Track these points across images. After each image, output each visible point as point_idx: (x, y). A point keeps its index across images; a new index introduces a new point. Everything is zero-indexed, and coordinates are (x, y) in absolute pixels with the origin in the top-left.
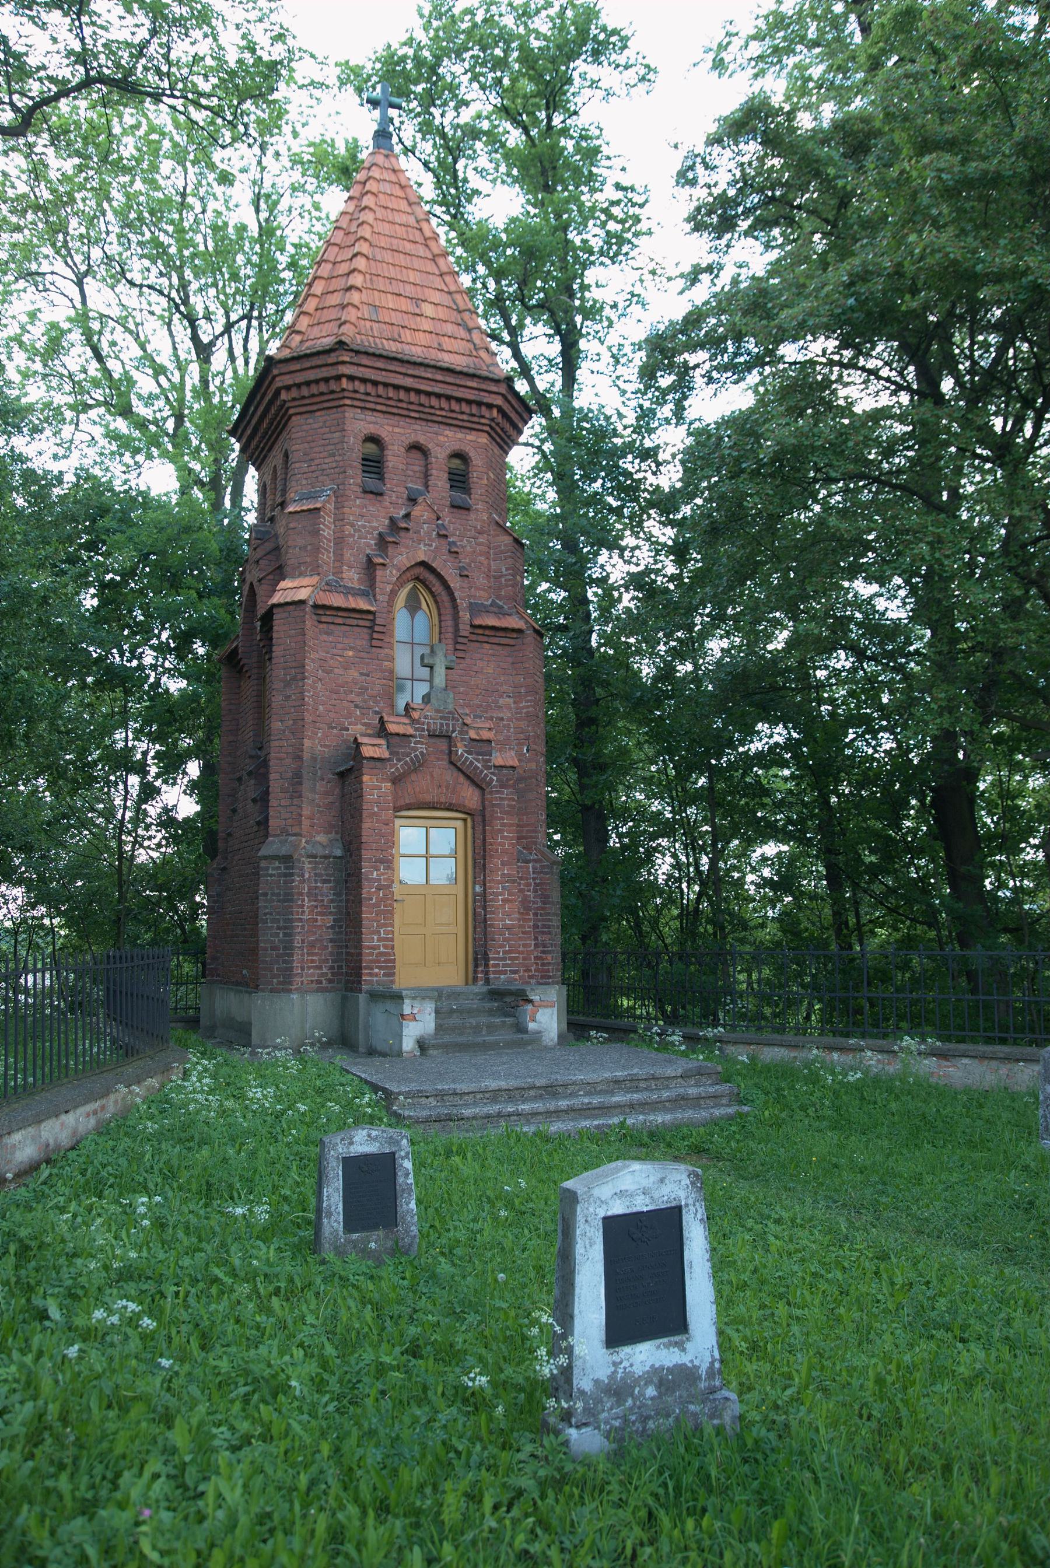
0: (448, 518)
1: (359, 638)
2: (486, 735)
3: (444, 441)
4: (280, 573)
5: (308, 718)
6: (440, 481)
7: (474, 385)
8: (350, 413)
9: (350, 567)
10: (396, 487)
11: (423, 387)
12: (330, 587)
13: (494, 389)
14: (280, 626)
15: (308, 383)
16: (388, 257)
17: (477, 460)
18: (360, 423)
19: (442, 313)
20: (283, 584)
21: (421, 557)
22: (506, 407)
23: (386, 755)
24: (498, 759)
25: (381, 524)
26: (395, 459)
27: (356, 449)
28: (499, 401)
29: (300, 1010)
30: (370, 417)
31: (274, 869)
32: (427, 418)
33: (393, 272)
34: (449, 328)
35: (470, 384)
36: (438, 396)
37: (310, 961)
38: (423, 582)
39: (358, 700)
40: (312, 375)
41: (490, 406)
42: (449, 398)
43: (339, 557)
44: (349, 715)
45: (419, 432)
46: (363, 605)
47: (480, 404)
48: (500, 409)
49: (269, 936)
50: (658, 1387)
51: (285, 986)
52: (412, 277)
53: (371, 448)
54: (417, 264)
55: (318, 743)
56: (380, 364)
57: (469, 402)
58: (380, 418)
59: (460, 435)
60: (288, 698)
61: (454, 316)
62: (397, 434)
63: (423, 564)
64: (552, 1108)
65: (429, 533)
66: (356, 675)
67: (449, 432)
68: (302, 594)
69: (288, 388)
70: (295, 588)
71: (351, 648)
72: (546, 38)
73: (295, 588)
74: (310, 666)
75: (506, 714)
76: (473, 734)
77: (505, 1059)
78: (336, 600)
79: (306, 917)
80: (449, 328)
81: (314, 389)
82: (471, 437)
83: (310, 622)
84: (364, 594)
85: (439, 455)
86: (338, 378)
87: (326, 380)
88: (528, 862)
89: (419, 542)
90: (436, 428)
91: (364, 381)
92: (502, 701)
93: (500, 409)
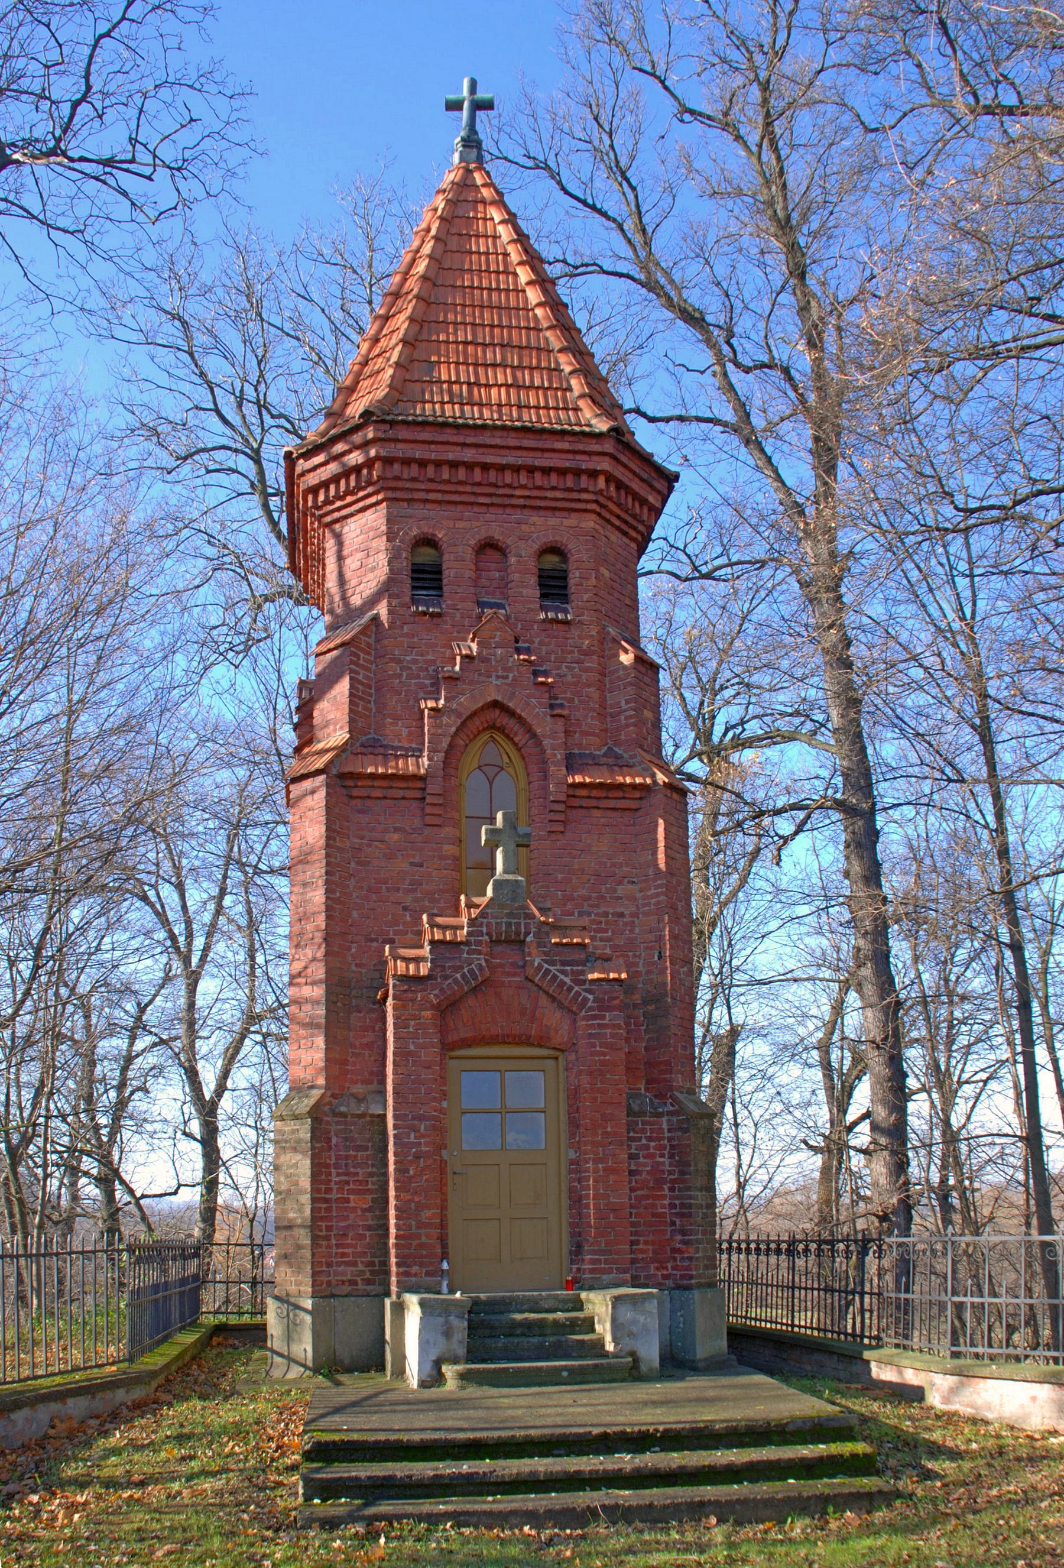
3: (527, 534)
7: (566, 446)
9: (396, 718)
11: (489, 459)
13: (597, 448)
17: (580, 553)
21: (493, 695)
22: (619, 473)
26: (456, 567)
28: (605, 465)
30: (419, 510)
35: (558, 445)
36: (517, 469)
38: (501, 730)
41: (593, 474)
42: (531, 470)
44: (395, 922)
47: (578, 473)
48: (609, 478)
56: (426, 435)
58: (434, 511)
59: (553, 521)
63: (495, 704)
64: (629, 1398)
66: (405, 866)
67: (535, 518)
71: (396, 830)
77: (661, 1428)
79: (334, 1196)
81: (492, 476)
82: (572, 520)
88: (660, 1115)
90: (518, 515)
92: (620, 890)
93: (609, 478)
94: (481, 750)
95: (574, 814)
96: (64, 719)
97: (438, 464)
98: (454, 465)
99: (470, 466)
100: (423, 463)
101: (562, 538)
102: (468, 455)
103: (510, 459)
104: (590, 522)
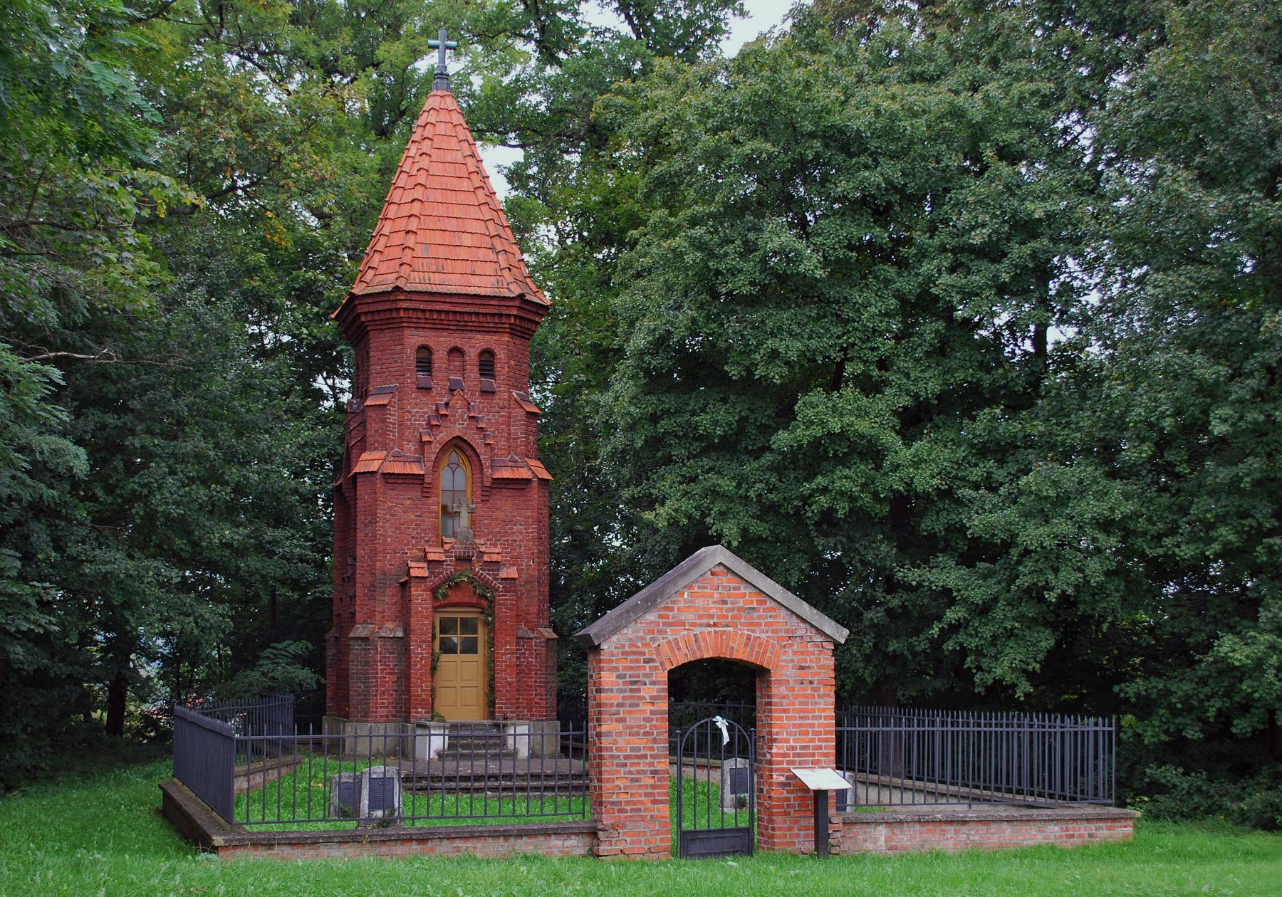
0: (477, 401)
1: (416, 493)
2: (496, 558)
3: (474, 344)
4: (363, 446)
5: (380, 548)
6: (473, 373)
8: (407, 332)
9: (409, 441)
10: (439, 384)
11: (457, 309)
12: (397, 458)
14: (362, 489)
15: (379, 312)
16: (438, 196)
17: (501, 354)
18: (414, 338)
19: (476, 241)
20: (365, 456)
21: (457, 433)
23: (426, 574)
24: (504, 574)
25: (429, 410)
27: (410, 354)
29: (369, 734)
30: (422, 333)
31: (356, 648)
32: (463, 329)
33: (441, 210)
34: (482, 254)
36: (470, 314)
37: (383, 703)
38: (460, 448)
39: (414, 534)
40: (380, 307)
41: (509, 316)
42: (477, 314)
43: (401, 435)
45: (457, 340)
46: (416, 470)
47: (500, 315)
49: (356, 687)
50: (1011, 227)
51: (365, 716)
52: (456, 211)
53: (424, 354)
54: (461, 198)
55: (387, 563)
56: (426, 298)
57: (493, 315)
59: (487, 337)
60: (366, 535)
61: (487, 242)
62: (441, 343)
65: (462, 416)
68: (374, 467)
69: (366, 313)
70: (370, 461)
72: (479, 98)
73: (370, 461)
74: (380, 513)
75: (518, 537)
76: (486, 558)
78: (397, 469)
80: (482, 254)
81: (383, 316)
83: (379, 484)
84: (419, 461)
85: (472, 354)
86: (398, 310)
87: (390, 310)
89: (455, 421)
91: (416, 310)
93: (516, 316)
94: (454, 456)
95: (494, 491)
96: (566, 633)
97: (431, 311)
98: (439, 312)
99: (447, 312)
100: (424, 311)
101: (432, 343)
102: (447, 307)
103: (468, 309)
104: (506, 338)
